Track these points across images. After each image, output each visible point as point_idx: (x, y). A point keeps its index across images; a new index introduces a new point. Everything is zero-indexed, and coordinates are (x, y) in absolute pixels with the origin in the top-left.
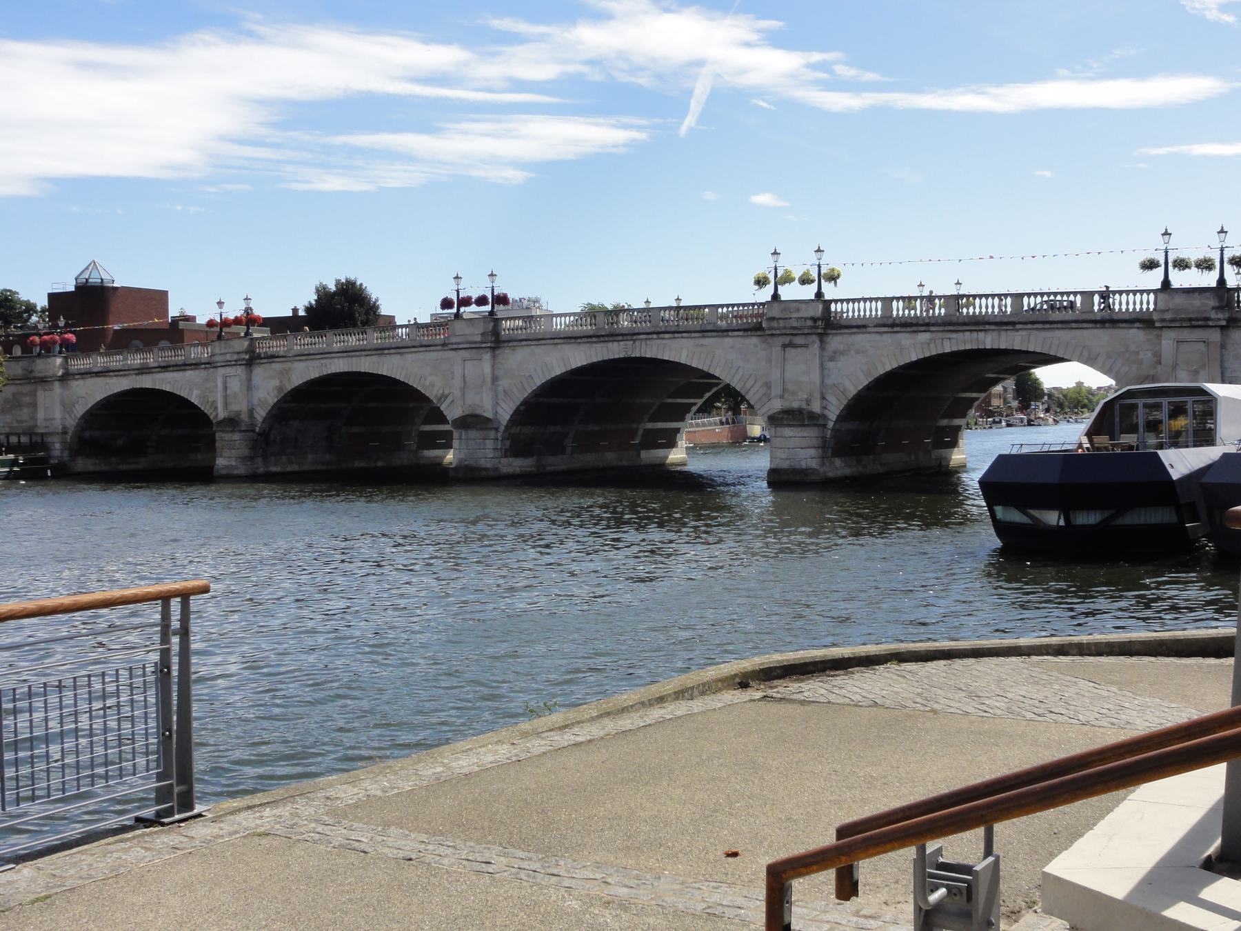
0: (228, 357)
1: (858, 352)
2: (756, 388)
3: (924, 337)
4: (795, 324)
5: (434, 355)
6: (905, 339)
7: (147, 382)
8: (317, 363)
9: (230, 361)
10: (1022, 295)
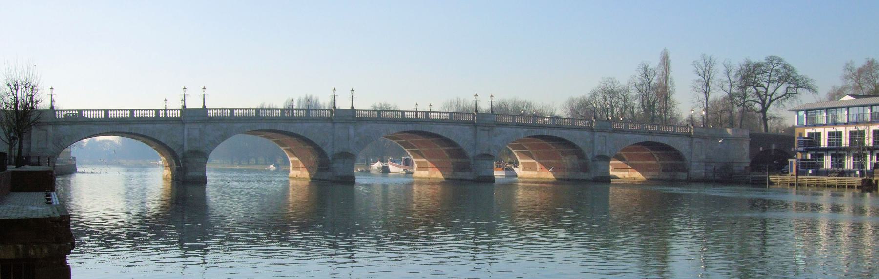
3: (526, 130)
10: (108, 110)
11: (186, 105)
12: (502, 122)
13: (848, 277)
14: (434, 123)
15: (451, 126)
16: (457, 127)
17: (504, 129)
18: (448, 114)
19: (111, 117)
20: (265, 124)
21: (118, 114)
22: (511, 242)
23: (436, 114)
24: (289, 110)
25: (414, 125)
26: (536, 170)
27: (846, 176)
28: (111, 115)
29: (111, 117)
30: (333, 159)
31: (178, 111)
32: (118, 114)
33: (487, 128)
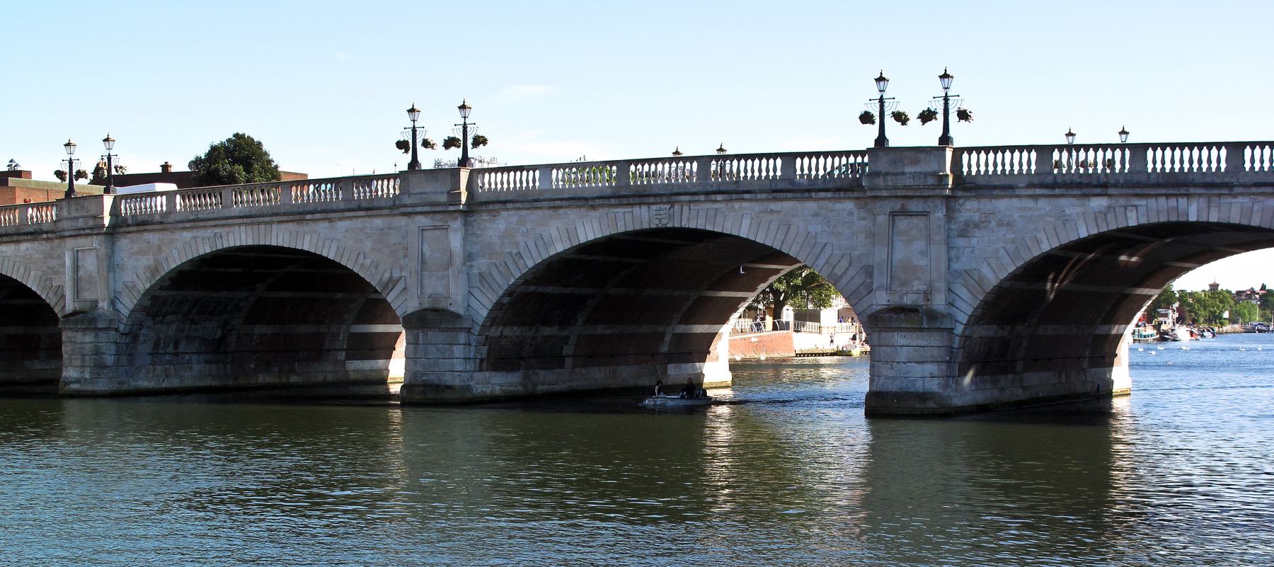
0: (81, 223)
1: (1000, 224)
2: (851, 273)
3: (1098, 203)
4: (909, 182)
5: (378, 222)
6: (1070, 205)
7: (281, 236)
8: (209, 232)
9: (84, 229)
10: (1242, 145)
11: (887, 135)
12: (271, 206)
13: (737, 563)
14: (719, 197)
15: (787, 205)
16: (811, 205)
17: (1003, 205)
18: (1267, 150)
19: (1154, 169)
20: (243, 228)
21: (1205, 158)
22: (1261, 371)
23: (1205, 151)
24: (266, 154)
25: (654, 207)
26: (561, 365)
27: (1119, 337)
28: (1154, 162)
29: (1154, 169)
30: (878, 288)
31: (1219, 149)
32: (1205, 158)
33: (915, 206)
